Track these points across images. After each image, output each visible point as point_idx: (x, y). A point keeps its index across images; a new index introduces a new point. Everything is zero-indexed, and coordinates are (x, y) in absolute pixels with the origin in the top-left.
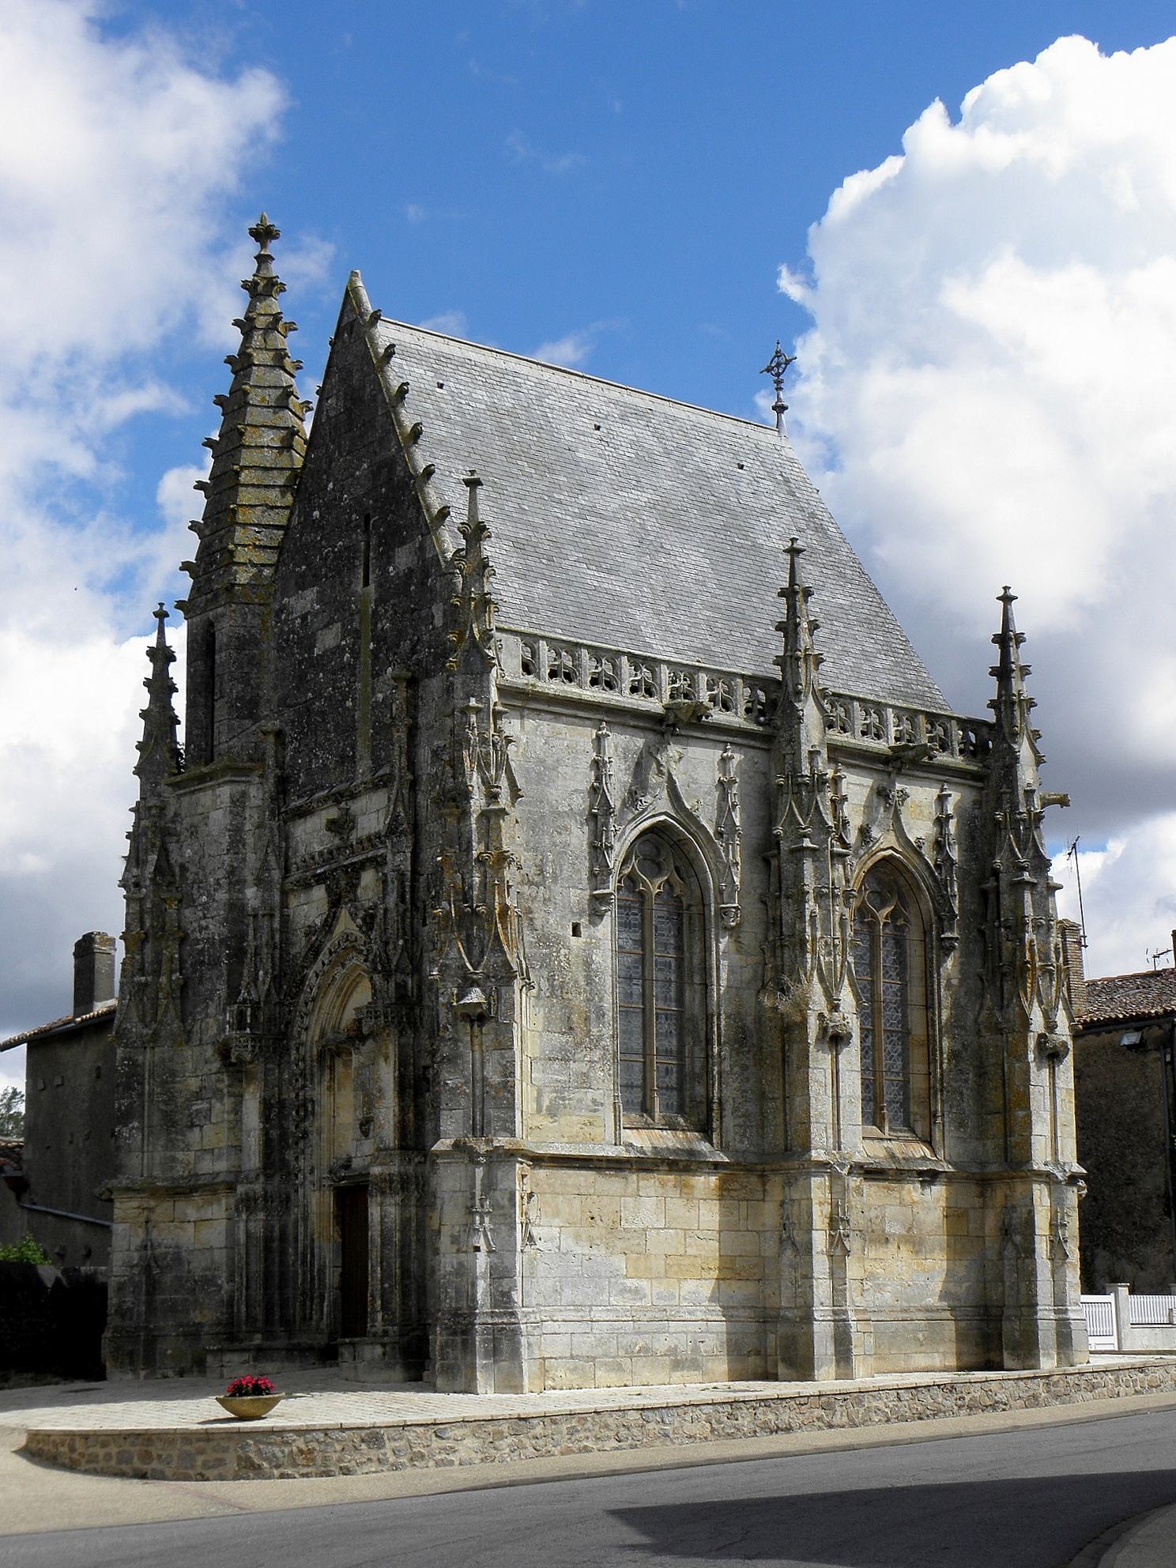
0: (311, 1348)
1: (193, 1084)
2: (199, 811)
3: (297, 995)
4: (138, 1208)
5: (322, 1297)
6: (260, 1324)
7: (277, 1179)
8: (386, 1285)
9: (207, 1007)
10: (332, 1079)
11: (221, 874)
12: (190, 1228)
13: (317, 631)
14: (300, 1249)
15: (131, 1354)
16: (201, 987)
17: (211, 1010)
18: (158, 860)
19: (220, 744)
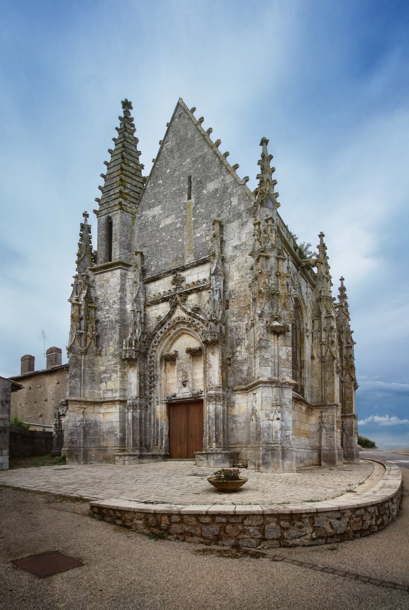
0: (160, 455)
1: (103, 369)
2: (105, 279)
3: (151, 340)
4: (79, 407)
5: (162, 439)
6: (138, 447)
7: (143, 399)
8: (217, 433)
9: (109, 343)
10: (165, 368)
11: (115, 299)
12: (101, 416)
13: (161, 219)
14: (152, 423)
15: (77, 456)
16: (106, 337)
17: (111, 344)
18: (87, 293)
19: (115, 256)
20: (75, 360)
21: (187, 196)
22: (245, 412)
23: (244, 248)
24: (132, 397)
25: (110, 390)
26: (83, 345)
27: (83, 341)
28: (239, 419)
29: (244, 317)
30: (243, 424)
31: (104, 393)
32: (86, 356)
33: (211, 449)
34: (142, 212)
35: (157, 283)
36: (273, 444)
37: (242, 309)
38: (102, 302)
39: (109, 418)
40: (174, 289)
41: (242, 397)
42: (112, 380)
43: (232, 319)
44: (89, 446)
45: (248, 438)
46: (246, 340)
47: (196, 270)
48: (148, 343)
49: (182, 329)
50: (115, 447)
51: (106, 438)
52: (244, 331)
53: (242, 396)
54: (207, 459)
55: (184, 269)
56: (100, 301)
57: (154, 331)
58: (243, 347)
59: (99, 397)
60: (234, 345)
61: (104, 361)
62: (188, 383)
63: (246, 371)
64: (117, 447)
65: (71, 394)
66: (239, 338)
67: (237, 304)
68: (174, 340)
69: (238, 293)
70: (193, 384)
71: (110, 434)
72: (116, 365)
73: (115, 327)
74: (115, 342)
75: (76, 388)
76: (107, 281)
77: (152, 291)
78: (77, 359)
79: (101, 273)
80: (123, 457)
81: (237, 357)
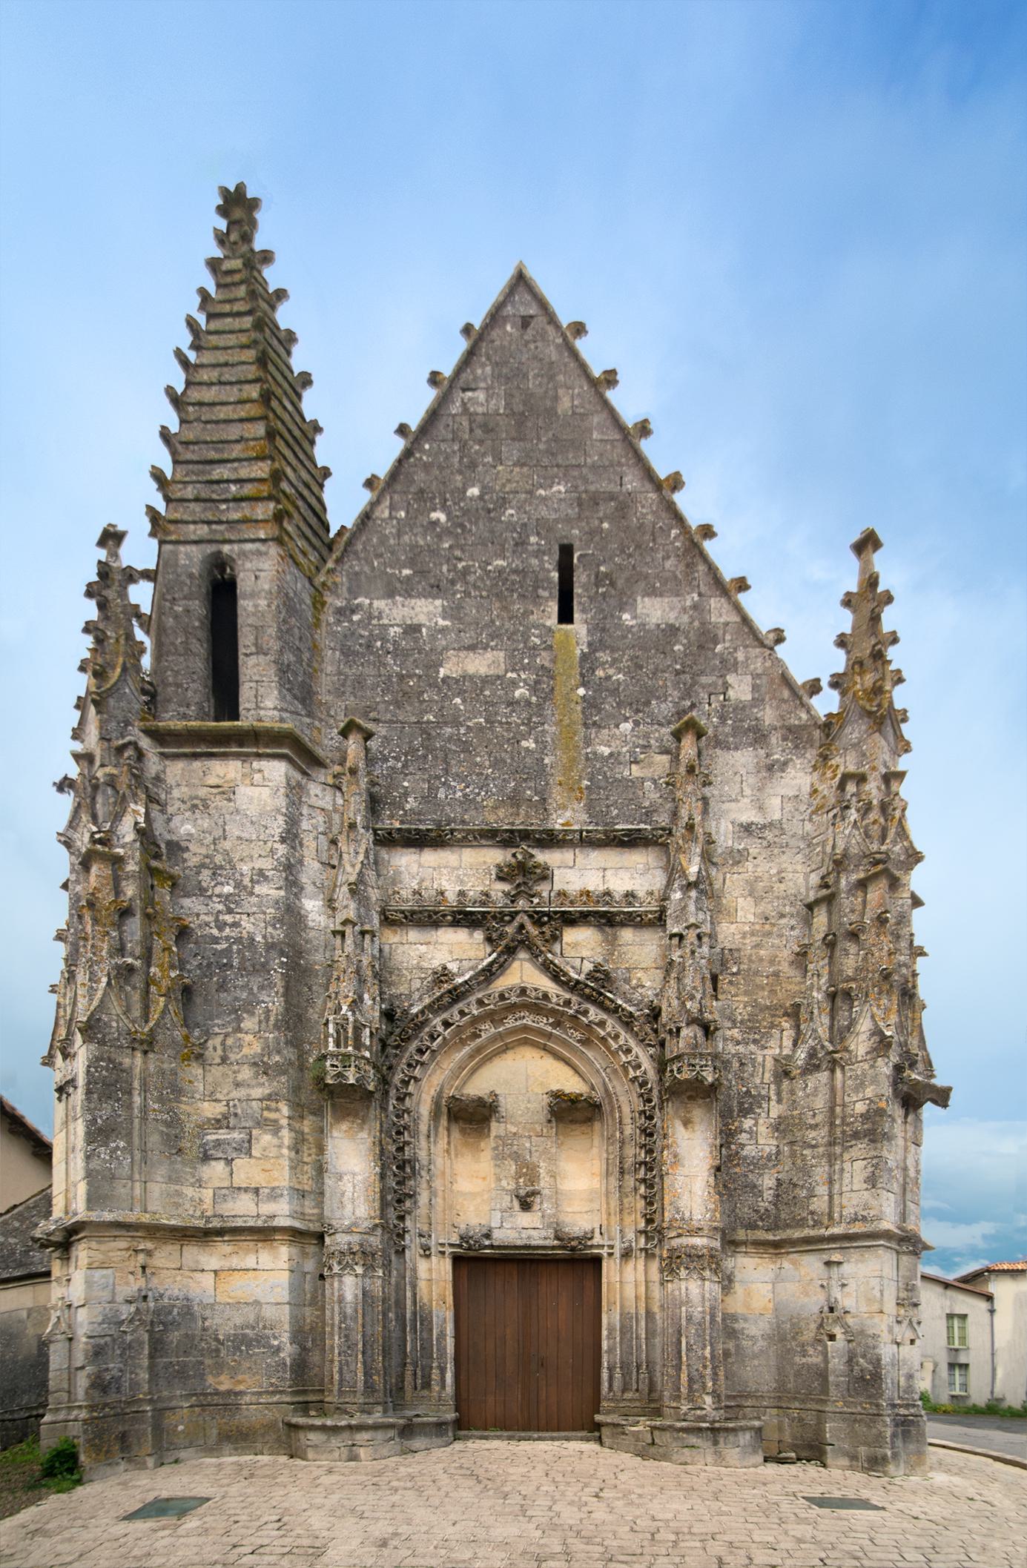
1: (211, 1110)
4: (128, 1249)
9: (239, 1020)
20: (107, 1069)
21: (553, 607)
22: (765, 1309)
23: (776, 839)
24: (355, 1224)
25: (246, 1190)
26: (136, 1013)
27: (136, 997)
28: (746, 1326)
29: (768, 1035)
30: (761, 1343)
31: (218, 1197)
32: (151, 1055)
33: (698, 1412)
34: (354, 593)
35: (430, 857)
36: (901, 1406)
37: (761, 1010)
38: (203, 866)
39: (240, 1288)
40: (506, 894)
41: (758, 1264)
42: (254, 1153)
43: (729, 1033)
44: (165, 1393)
45: (777, 1381)
46: (773, 1103)
47: (597, 858)
48: (397, 1047)
49: (526, 1028)
50: (274, 1393)
51: (229, 1359)
52: (767, 1075)
53: (759, 1261)
55: (551, 840)
56: (193, 861)
57: (422, 1012)
58: (761, 1121)
59: (198, 1213)
60: (731, 1111)
61: (216, 1084)
63: (771, 1192)
64: (281, 1392)
65: (92, 1201)
66: (748, 1092)
67: (746, 993)
68: (483, 1057)
69: (750, 961)
72: (273, 1105)
73: (263, 965)
74: (267, 1019)
75: (113, 1177)
76: (228, 792)
78: (118, 1068)
79: (195, 756)
80: (346, 1435)
81: (742, 1146)
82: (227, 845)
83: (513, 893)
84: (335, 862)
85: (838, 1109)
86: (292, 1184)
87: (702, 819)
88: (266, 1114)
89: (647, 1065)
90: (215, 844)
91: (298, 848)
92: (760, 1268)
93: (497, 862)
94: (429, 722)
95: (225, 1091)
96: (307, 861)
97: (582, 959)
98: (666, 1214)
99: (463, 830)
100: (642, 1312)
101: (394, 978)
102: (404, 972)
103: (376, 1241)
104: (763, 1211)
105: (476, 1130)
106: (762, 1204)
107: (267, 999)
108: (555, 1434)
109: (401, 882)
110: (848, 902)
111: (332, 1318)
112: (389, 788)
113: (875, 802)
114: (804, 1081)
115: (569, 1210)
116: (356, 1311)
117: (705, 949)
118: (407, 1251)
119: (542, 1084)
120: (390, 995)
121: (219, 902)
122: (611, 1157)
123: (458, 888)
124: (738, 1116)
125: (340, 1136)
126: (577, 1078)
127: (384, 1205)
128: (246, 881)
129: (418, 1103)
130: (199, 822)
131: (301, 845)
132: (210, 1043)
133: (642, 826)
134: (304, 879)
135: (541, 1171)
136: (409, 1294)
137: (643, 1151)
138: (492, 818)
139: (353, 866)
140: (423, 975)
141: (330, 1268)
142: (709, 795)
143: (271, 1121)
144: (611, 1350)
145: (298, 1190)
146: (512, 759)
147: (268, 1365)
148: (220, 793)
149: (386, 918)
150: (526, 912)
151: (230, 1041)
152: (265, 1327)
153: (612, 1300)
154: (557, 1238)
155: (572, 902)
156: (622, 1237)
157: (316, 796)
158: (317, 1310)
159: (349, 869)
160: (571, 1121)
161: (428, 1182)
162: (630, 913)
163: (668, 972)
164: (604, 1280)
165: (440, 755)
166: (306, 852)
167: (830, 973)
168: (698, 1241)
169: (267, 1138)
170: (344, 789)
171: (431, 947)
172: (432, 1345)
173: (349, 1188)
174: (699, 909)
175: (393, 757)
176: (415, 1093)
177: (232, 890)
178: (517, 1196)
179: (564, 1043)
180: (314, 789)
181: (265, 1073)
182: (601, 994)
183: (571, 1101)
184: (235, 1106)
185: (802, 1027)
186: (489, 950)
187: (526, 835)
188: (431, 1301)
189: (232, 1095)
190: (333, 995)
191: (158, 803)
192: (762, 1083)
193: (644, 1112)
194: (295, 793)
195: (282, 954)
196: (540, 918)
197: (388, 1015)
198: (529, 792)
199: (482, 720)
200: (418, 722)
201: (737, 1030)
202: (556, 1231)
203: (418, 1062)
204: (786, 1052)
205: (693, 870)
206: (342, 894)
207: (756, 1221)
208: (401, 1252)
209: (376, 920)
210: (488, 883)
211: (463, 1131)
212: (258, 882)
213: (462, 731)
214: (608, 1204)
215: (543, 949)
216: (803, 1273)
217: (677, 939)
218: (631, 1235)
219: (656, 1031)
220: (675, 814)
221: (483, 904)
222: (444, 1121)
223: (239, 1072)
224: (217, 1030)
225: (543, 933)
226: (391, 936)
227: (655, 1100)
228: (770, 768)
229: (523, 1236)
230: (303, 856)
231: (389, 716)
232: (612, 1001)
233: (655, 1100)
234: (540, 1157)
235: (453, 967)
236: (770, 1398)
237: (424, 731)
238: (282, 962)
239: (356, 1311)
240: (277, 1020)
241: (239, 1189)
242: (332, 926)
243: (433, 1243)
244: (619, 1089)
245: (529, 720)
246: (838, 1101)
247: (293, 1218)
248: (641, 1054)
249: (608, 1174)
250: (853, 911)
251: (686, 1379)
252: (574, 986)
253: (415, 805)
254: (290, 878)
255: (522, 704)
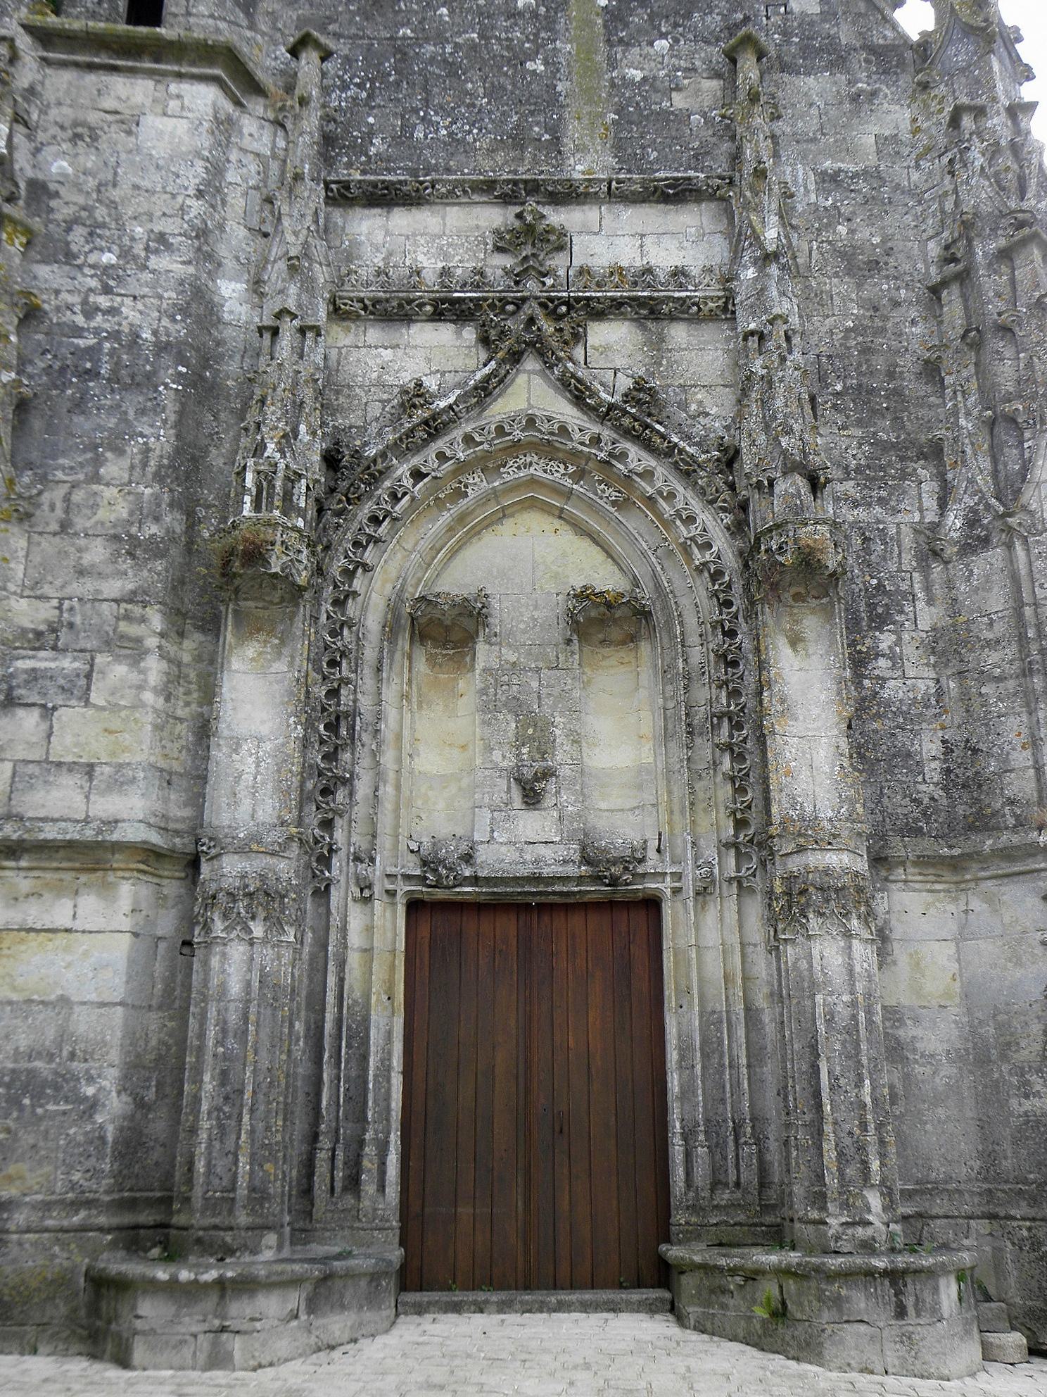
9: (98, 461)
22: (947, 994)
25: (71, 767)
28: (918, 1032)
33: (860, 1232)
35: (401, 220)
40: (507, 272)
41: (928, 905)
42: (95, 697)
43: (840, 488)
46: (920, 605)
47: (632, 217)
48: (338, 514)
49: (533, 482)
50: (75, 1205)
53: (929, 897)
54: (901, 1312)
55: (568, 195)
56: (63, 211)
57: (383, 455)
62: (552, 787)
63: (936, 765)
64: (89, 1204)
66: (880, 586)
67: (859, 423)
70: (583, 795)
71: (38, 1097)
72: (137, 610)
73: (148, 376)
74: (145, 465)
76: (129, 123)
77: (367, 250)
79: (91, 67)
81: (881, 680)
82: (115, 194)
83: (517, 270)
84: (268, 228)
85: (1028, 611)
86: (152, 759)
87: (774, 163)
88: (123, 627)
89: (721, 542)
90: (99, 191)
91: (220, 208)
92: (932, 911)
93: (495, 226)
94: (405, 38)
95: (58, 582)
96: (231, 225)
97: (616, 371)
98: (774, 809)
99: (450, 181)
100: (739, 1008)
101: (342, 400)
102: (358, 390)
103: (286, 868)
104: (926, 801)
105: (451, 658)
106: (923, 787)
107: (147, 430)
108: (588, 1296)
109: (359, 257)
110: (990, 283)
111: (202, 1035)
112: (347, 128)
113: (1003, 143)
114: (967, 565)
115: (603, 805)
116: (245, 1018)
117: (797, 355)
118: (332, 888)
119: (556, 576)
120: (334, 426)
121: (92, 276)
122: (671, 704)
123: (440, 265)
124: (870, 628)
125: (243, 668)
126: (610, 565)
127: (304, 798)
128: (139, 249)
129: (364, 610)
130: (81, 159)
131: (224, 203)
132: (46, 497)
133: (691, 173)
134: (223, 251)
135: (558, 732)
136: (332, 981)
137: (724, 694)
138: (487, 164)
139: (296, 234)
140: (385, 396)
141: (207, 928)
142: (779, 133)
143: (130, 639)
144: (687, 1092)
145: (161, 770)
146: (514, 85)
147: (71, 1141)
148: (117, 122)
149: (336, 309)
150: (536, 298)
151: (78, 496)
152: (72, 1056)
153: (683, 983)
154: (586, 860)
155: (598, 285)
156: (696, 858)
157: (251, 135)
158: (171, 1019)
159: (290, 238)
160: (603, 642)
161: (374, 754)
162: (682, 301)
163: (745, 393)
164: (667, 943)
165: (418, 79)
166: (229, 214)
167: (981, 390)
168: (834, 860)
169: (120, 670)
170: (289, 126)
171: (400, 352)
172: (366, 1090)
173: (249, 765)
174: (783, 294)
175: (356, 85)
176: (362, 592)
177: (114, 260)
178: (518, 781)
179: (592, 506)
180: (249, 125)
181: (129, 553)
182: (647, 426)
183: (609, 605)
184: (71, 609)
185: (950, 476)
186: (483, 356)
187: (533, 187)
188: (367, 996)
189: (68, 591)
190: (252, 427)
191: (26, 125)
192: (899, 571)
193: (722, 623)
194: (224, 128)
195: (182, 360)
196: (556, 307)
197: (331, 461)
198: (536, 129)
199: (475, 35)
200: (391, 38)
201: (852, 483)
202: (583, 849)
203: (370, 538)
204: (931, 517)
205: (771, 234)
206: (276, 272)
207: (916, 820)
208: (322, 894)
209: (322, 311)
210: (482, 256)
211: (431, 660)
212: (157, 252)
213: (449, 49)
214: (670, 793)
215: (562, 354)
216: (1007, 920)
217: (756, 338)
218: (710, 853)
219: (732, 487)
220: (736, 158)
221: (477, 287)
222: (404, 642)
223: (87, 549)
224: (60, 475)
225: (561, 330)
226: (341, 335)
227: (738, 604)
228: (855, 98)
229: (528, 857)
230: (225, 219)
231: (353, 31)
232: (663, 437)
233: (738, 604)
234: (554, 707)
235: (431, 383)
236: (972, 1193)
237: (398, 50)
238: (180, 374)
239: (245, 1018)
240: (160, 466)
241: (59, 764)
242: (257, 319)
243: (376, 872)
244: (679, 585)
245: (536, 35)
246: (1026, 597)
247: (149, 825)
248: (710, 524)
249: (667, 736)
250: (998, 295)
251: (834, 1155)
252: (606, 414)
253: (383, 148)
254: (205, 248)
255: (527, 16)
